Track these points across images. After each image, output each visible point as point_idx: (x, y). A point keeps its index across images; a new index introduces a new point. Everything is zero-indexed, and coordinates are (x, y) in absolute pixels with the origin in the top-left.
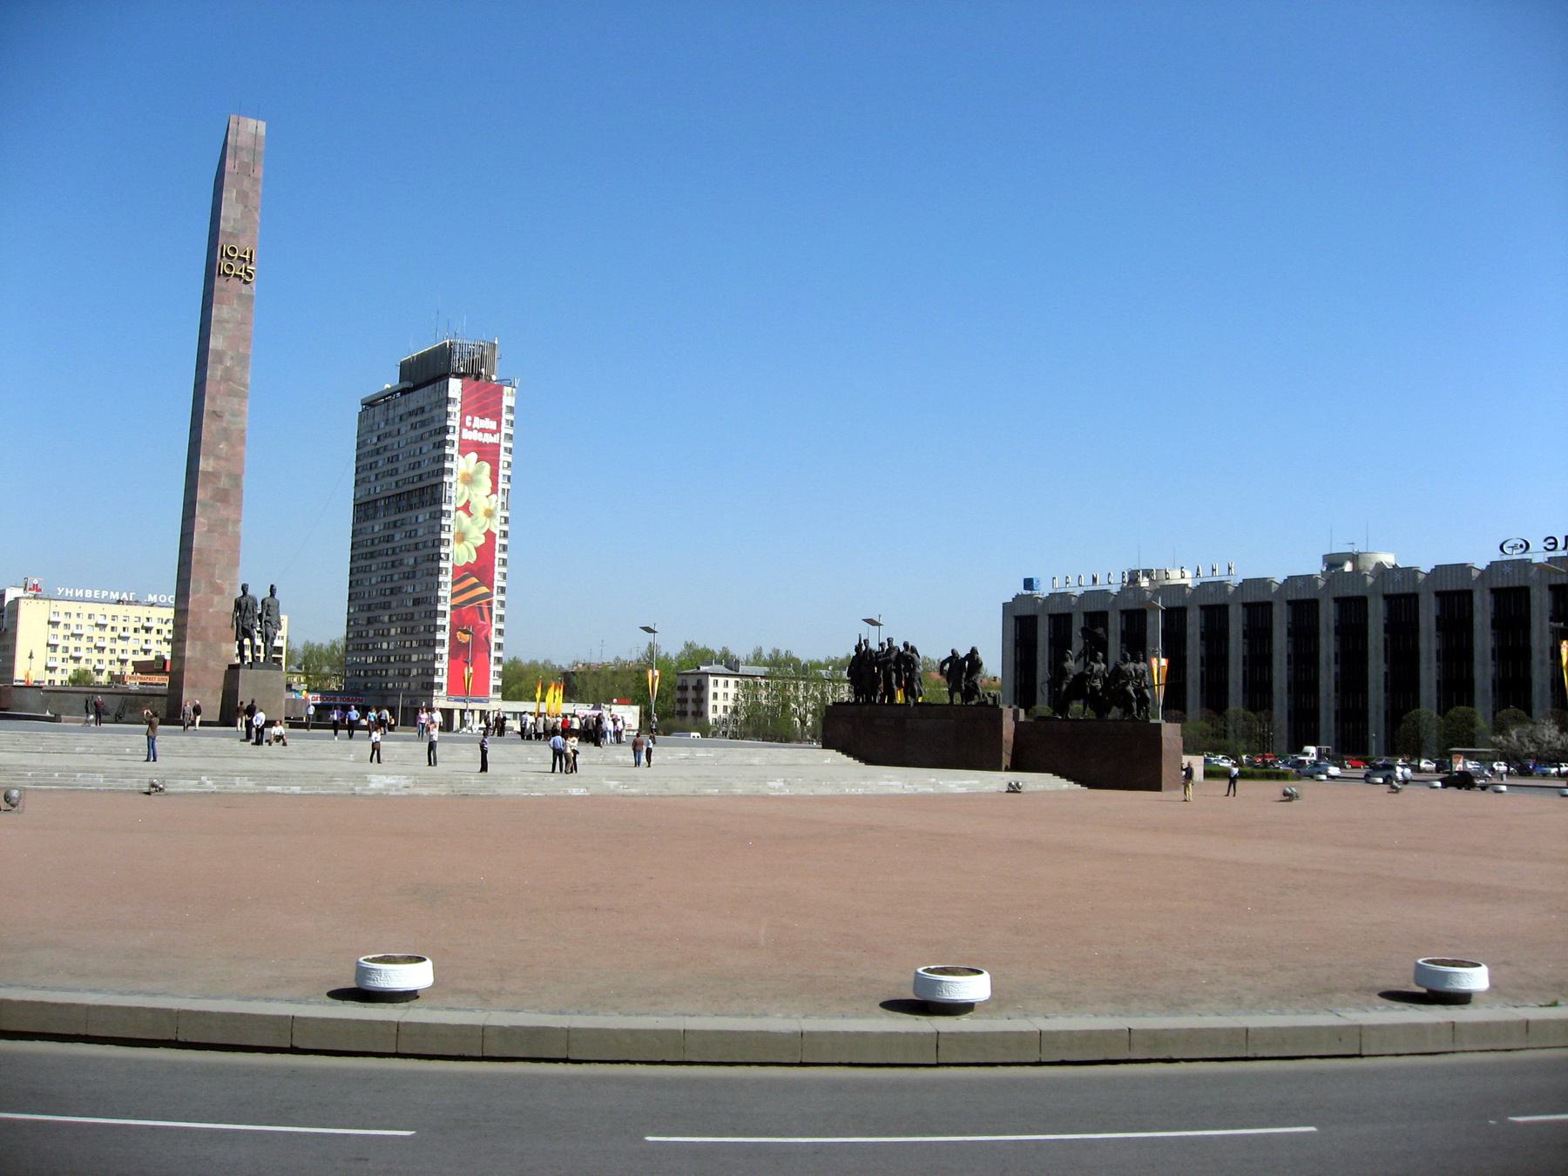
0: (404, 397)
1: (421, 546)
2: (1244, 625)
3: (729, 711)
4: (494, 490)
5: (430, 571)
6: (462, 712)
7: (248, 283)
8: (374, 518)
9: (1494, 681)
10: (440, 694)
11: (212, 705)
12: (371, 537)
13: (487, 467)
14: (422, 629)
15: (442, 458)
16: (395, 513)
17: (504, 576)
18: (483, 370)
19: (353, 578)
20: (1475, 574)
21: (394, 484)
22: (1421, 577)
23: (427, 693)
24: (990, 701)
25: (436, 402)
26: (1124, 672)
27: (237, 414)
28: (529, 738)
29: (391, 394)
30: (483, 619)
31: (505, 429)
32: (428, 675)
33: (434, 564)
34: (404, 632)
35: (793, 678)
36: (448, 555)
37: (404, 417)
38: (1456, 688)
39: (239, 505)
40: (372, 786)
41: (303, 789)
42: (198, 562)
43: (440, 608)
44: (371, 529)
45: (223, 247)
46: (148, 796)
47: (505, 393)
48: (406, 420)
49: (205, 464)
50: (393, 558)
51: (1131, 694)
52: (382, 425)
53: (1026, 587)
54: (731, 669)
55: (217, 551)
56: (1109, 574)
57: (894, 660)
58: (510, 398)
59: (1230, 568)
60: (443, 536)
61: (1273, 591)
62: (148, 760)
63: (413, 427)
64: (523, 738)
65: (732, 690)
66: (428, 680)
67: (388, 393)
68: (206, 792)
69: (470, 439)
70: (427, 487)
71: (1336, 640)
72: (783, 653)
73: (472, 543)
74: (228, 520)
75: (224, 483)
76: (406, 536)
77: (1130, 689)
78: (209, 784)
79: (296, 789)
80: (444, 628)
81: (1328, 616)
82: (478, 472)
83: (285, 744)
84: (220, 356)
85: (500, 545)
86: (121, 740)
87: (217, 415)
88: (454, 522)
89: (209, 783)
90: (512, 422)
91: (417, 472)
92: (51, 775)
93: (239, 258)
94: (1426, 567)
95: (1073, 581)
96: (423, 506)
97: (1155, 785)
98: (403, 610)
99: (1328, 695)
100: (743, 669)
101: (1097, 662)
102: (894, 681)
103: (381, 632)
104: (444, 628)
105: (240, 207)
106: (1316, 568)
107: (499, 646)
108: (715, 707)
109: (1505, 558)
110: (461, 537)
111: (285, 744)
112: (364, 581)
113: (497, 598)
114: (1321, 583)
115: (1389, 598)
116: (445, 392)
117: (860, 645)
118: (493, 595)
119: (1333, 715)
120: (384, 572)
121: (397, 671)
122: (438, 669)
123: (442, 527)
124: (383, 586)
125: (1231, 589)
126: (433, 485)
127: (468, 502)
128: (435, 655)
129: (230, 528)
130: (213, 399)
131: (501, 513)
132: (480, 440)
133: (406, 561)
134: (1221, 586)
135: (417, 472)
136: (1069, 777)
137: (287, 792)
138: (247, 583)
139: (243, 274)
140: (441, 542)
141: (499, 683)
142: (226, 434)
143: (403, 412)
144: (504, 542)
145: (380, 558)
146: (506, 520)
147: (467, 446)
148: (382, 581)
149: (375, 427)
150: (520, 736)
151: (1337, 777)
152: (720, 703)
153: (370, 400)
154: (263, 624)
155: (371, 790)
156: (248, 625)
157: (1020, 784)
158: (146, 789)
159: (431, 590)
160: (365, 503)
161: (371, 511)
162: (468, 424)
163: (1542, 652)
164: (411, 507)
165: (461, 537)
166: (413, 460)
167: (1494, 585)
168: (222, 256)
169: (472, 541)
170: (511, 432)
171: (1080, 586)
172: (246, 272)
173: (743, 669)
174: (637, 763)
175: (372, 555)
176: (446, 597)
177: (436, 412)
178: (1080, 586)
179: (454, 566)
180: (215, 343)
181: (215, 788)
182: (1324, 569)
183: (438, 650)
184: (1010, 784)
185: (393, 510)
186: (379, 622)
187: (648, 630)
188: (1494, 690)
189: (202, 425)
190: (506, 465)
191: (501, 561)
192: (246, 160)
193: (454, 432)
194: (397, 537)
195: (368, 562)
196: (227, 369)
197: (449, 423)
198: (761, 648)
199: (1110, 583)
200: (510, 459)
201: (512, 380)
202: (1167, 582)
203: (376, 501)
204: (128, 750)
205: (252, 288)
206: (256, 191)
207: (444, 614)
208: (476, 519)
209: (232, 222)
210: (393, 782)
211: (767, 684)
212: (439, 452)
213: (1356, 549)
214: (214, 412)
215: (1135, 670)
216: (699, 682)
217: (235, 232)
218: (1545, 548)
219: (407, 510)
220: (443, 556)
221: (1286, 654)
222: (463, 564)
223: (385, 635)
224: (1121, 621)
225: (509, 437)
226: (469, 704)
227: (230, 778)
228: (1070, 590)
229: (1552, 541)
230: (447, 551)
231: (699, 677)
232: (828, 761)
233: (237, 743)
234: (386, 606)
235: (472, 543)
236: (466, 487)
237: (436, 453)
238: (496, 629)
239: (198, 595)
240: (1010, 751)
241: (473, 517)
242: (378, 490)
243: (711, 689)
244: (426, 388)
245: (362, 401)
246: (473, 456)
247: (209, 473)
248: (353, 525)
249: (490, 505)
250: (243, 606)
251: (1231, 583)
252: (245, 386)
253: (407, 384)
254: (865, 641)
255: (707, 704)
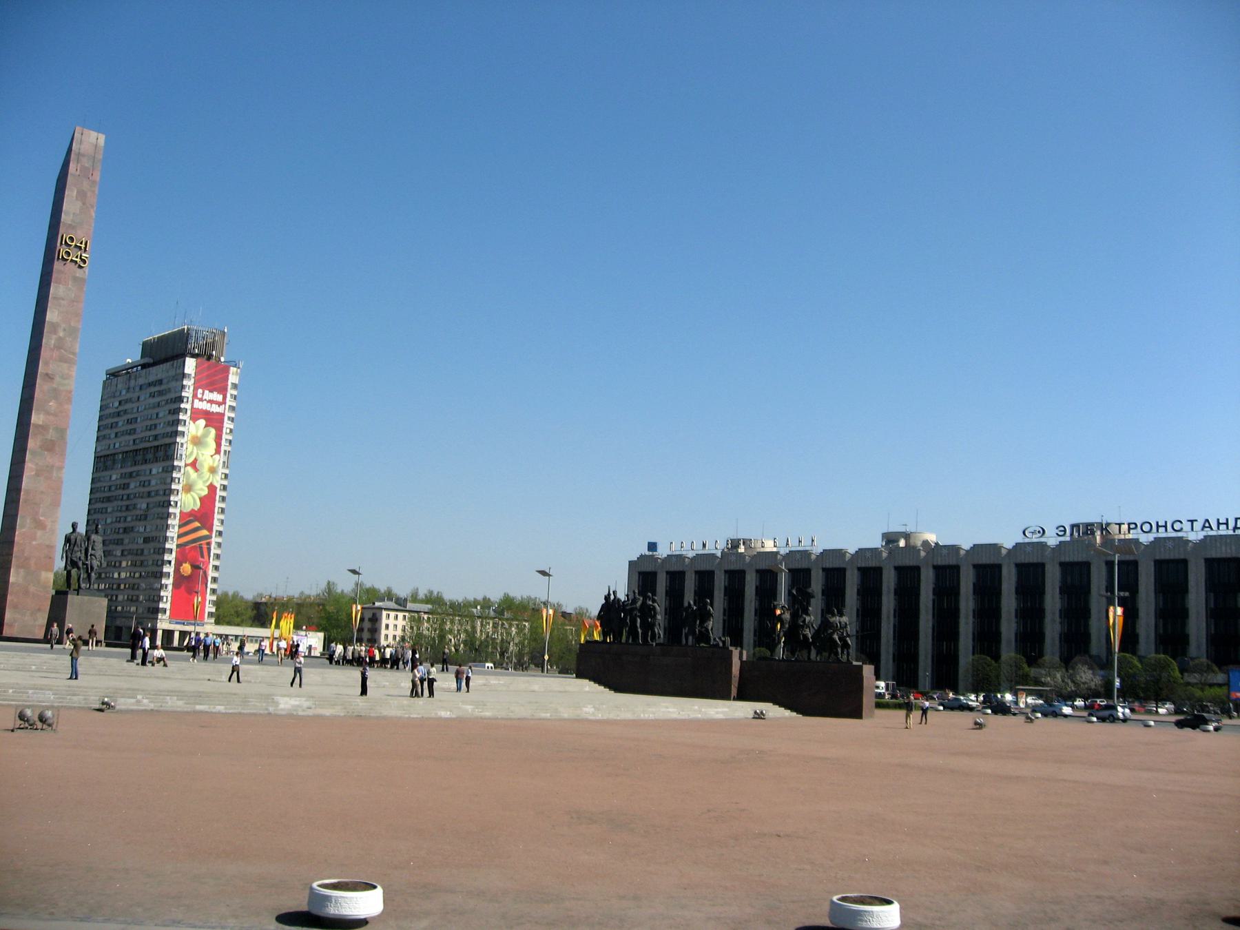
0: (144, 370)
1: (153, 494)
2: (823, 585)
3: (398, 639)
4: (218, 451)
5: (160, 515)
6: (181, 632)
7: (82, 267)
8: (112, 469)
9: (1016, 634)
10: (164, 617)
11: (37, 623)
12: (109, 484)
13: (213, 432)
14: (150, 563)
15: (176, 422)
16: (131, 466)
17: (222, 522)
18: (214, 352)
19: (90, 517)
20: (1004, 552)
21: (131, 442)
22: (962, 552)
23: (151, 616)
24: (721, 645)
25: (173, 377)
26: (832, 623)
27: (66, 377)
28: (338, 663)
29: (132, 368)
30: (203, 557)
31: (230, 402)
32: (153, 601)
33: (164, 510)
34: (134, 565)
35: (450, 615)
36: (177, 502)
37: (144, 387)
38: (987, 640)
39: (63, 454)
40: (282, 706)
41: (226, 708)
42: (25, 501)
43: (167, 546)
44: (109, 477)
45: (63, 236)
46: (101, 713)
47: (231, 372)
48: (146, 389)
49: (36, 418)
50: (127, 503)
51: (836, 641)
52: (124, 392)
53: (649, 549)
54: (400, 605)
55: (42, 492)
56: (716, 541)
57: (638, 608)
58: (234, 377)
59: (813, 541)
60: (173, 487)
61: (847, 560)
62: (71, 678)
63: (152, 395)
64: (331, 663)
65: (401, 623)
66: (154, 605)
67: (130, 366)
68: (146, 710)
69: (200, 408)
70: (161, 445)
71: (895, 599)
72: (435, 593)
73: (197, 494)
74: (53, 466)
75: (51, 434)
76: (140, 485)
77: (836, 637)
78: (147, 704)
79: (221, 708)
80: (170, 562)
81: (889, 581)
82: (206, 435)
83: (165, 665)
84: (55, 327)
85: (220, 496)
86: (25, 658)
87: (49, 377)
88: (183, 475)
89: (145, 701)
90: (235, 396)
91: (153, 433)
92: (5, 691)
93: (76, 246)
94: (966, 545)
95: (687, 546)
96: (157, 461)
97: (857, 713)
98: (135, 547)
99: (888, 641)
100: (410, 606)
101: (808, 614)
102: (638, 625)
103: (113, 563)
104: (170, 562)
105: (79, 204)
106: (876, 542)
107: (215, 580)
108: (387, 636)
109: (1027, 540)
110: (189, 488)
111: (165, 665)
112: (101, 521)
113: (215, 539)
114: (885, 555)
115: (937, 568)
116: (181, 370)
117: (609, 594)
118: (212, 537)
119: (891, 657)
120: (119, 514)
121: (126, 597)
122: (163, 597)
123: (172, 480)
124: (118, 525)
125: (813, 557)
126: (166, 445)
127: (195, 460)
128: (162, 586)
129: (55, 474)
130: (47, 364)
131: (221, 470)
132: (208, 409)
133: (139, 506)
134: (806, 554)
135: (153, 433)
136: (787, 707)
137: (214, 711)
138: (76, 521)
139: (78, 260)
140: (171, 492)
141: (213, 610)
142: (55, 394)
143: (143, 383)
144: (224, 494)
145: (116, 502)
146: (226, 476)
147: (196, 415)
148: (116, 521)
149: (118, 394)
150: (328, 662)
151: (1070, 716)
152: (391, 632)
153: (113, 371)
154: (89, 557)
155: (282, 710)
156: (76, 557)
157: (764, 712)
158: (97, 706)
159: (160, 530)
160: (105, 456)
161: (109, 463)
162: (200, 396)
163: (1054, 614)
164: (145, 462)
165: (189, 488)
166: (149, 423)
167: (1018, 561)
168: (61, 244)
169: (198, 492)
170: (234, 404)
171: (692, 550)
172: (81, 258)
173: (410, 606)
174: (459, 689)
175: (109, 499)
176: (173, 538)
177: (173, 384)
178: (692, 550)
179: (181, 512)
180: (51, 316)
181: (152, 706)
182: (884, 544)
183: (164, 581)
184: (756, 712)
185: (129, 464)
186: (112, 555)
187: (354, 572)
188: (1016, 641)
189: (35, 384)
190: (228, 431)
191: (220, 510)
192: (86, 165)
193: (187, 402)
194: (132, 486)
195: (104, 505)
196: (60, 339)
197: (184, 394)
198: (417, 589)
199: (716, 548)
200: (232, 427)
201: (237, 362)
202: (762, 550)
203: (115, 454)
204: (34, 667)
205: (85, 272)
206: (94, 192)
207: (171, 551)
208: (202, 473)
209: (72, 215)
210: (297, 703)
211: (429, 618)
212: (174, 417)
213: (909, 529)
214: (47, 374)
215: (840, 623)
216: (374, 615)
217: (74, 224)
218: (1057, 534)
219: (142, 464)
220: (172, 503)
221: (855, 609)
222: (189, 510)
223: (117, 566)
224: (725, 578)
225: (232, 408)
226: (197, 627)
227: (161, 697)
228: (684, 553)
229: (1062, 529)
230: (176, 499)
231: (374, 611)
232: (587, 689)
233: (126, 664)
234: (119, 542)
235: (197, 494)
236: (195, 448)
237: (171, 418)
238: (213, 566)
239: (24, 530)
240: (737, 685)
241: (199, 473)
242: (117, 445)
243: (384, 621)
244: (165, 364)
245: (106, 372)
246: (202, 422)
247: (40, 426)
248: (93, 474)
249: (214, 462)
250: (73, 541)
251: (814, 552)
252: (74, 354)
253: (147, 360)
254: (614, 592)
255: (380, 633)
